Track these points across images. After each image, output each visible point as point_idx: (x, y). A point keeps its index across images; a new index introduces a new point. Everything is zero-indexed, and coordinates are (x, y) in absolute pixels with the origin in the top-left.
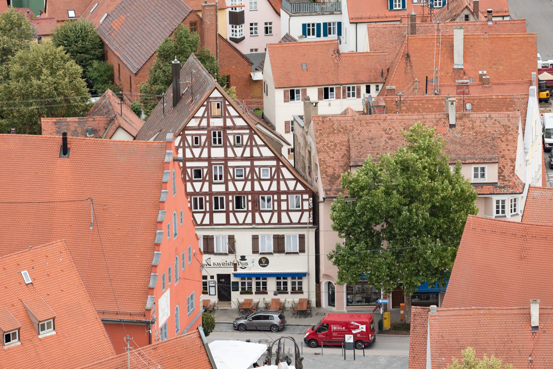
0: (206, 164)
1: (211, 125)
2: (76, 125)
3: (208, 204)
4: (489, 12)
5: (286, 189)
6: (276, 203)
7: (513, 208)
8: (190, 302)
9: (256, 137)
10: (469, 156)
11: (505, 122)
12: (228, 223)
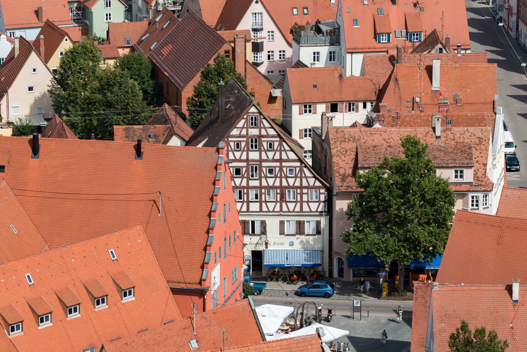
0: (244, 164)
1: (249, 134)
2: (141, 131)
3: (245, 196)
4: (458, 46)
5: (307, 185)
6: (299, 196)
7: (485, 202)
8: (234, 273)
9: (284, 143)
10: (451, 161)
11: (480, 135)
12: (261, 210)
